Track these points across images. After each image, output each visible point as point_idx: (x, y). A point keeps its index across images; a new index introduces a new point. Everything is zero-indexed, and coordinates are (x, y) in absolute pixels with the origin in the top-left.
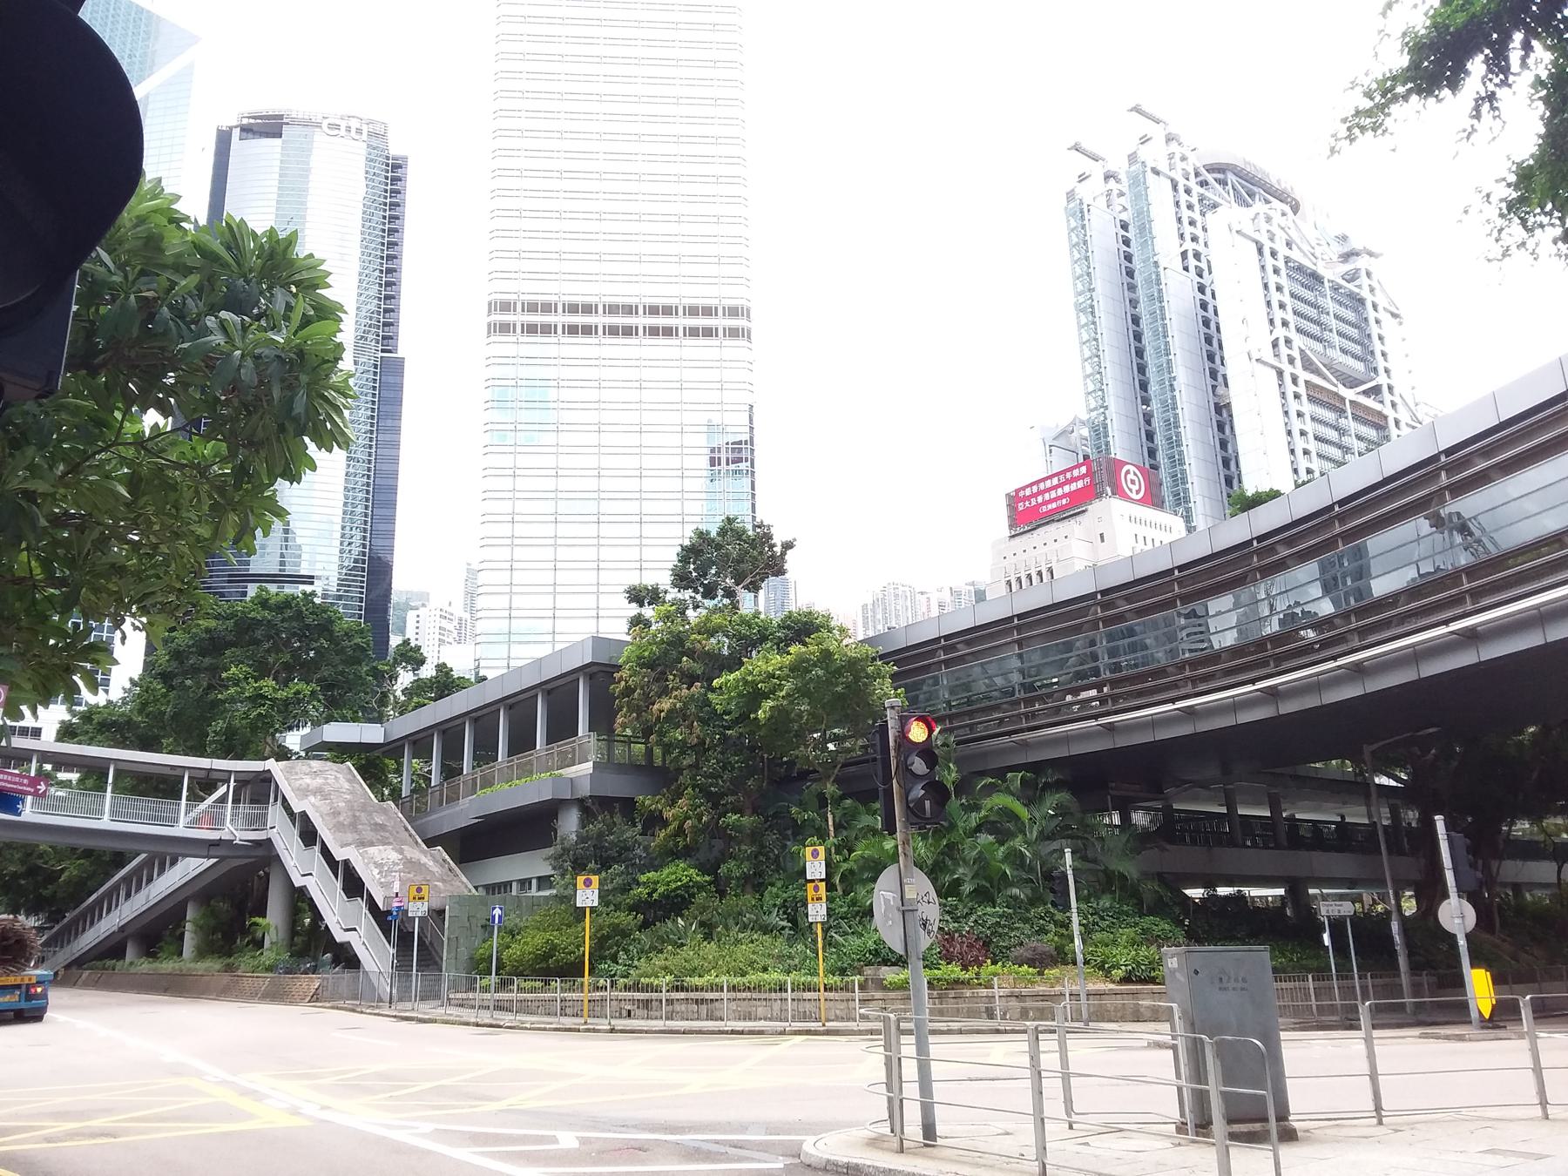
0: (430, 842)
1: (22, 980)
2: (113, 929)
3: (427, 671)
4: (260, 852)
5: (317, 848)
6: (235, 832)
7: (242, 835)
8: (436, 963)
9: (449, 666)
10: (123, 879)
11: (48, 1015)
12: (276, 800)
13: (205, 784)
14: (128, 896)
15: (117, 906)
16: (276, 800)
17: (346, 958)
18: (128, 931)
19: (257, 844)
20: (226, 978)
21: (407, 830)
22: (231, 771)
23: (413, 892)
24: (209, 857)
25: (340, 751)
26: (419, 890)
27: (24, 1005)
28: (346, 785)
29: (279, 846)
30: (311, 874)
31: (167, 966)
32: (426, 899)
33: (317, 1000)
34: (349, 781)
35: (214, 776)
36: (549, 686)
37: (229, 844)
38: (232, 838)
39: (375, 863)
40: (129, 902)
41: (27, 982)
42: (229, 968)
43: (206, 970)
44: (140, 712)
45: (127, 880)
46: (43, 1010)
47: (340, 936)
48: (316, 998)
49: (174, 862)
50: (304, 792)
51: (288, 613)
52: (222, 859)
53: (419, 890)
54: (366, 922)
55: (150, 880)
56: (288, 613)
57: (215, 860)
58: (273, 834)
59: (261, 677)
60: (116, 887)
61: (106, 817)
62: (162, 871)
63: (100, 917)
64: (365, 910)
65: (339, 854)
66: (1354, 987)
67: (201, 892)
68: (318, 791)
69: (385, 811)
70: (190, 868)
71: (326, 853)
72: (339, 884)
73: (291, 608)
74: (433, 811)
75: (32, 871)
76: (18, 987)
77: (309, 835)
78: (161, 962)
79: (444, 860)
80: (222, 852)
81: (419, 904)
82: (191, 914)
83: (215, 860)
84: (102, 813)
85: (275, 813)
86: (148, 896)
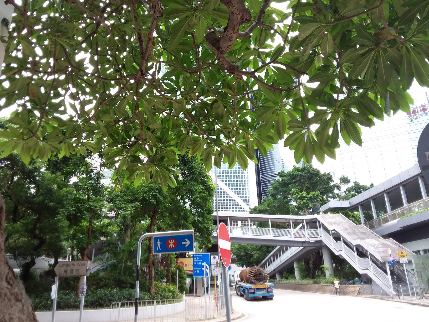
0: (386, 237)
1: (266, 286)
2: (271, 271)
3: (351, 185)
4: (318, 245)
5: (342, 242)
6: (310, 238)
7: (312, 240)
8: (403, 281)
9: (358, 182)
10: (272, 256)
11: (274, 298)
12: (320, 227)
13: (296, 224)
14: (274, 260)
15: (271, 263)
16: (320, 227)
17: (368, 280)
18: (276, 271)
19: (317, 242)
20: (316, 286)
21: (373, 234)
22: (60, 307)
23: (400, 254)
24: (300, 247)
25: (335, 210)
26: (402, 253)
27: (267, 295)
28: (343, 221)
29: (326, 242)
30: (342, 251)
31: (292, 281)
32: (406, 256)
33: (360, 294)
34: (344, 219)
35: (298, 221)
36: (404, 183)
37: (308, 242)
38: (309, 240)
39: (371, 245)
40: (275, 262)
41: (267, 287)
42: (315, 282)
43: (307, 283)
44: (268, 207)
45: (273, 256)
46: (272, 296)
47: (361, 272)
48: (359, 293)
49: (287, 249)
50: (331, 224)
51: (306, 171)
52: (304, 247)
53: (402, 253)
54: (372, 266)
55: (280, 255)
56: (306, 171)
57: (302, 248)
58: (322, 238)
59: (301, 192)
60: (270, 258)
61: (271, 235)
62: (283, 252)
63: (267, 267)
64: (371, 262)
65: (354, 242)
66: (179, 278)
67: (298, 258)
68: (335, 223)
69: (362, 228)
70: (293, 251)
71: (346, 243)
72: (355, 254)
73: (306, 170)
74: (377, 228)
75: (247, 254)
76: (265, 288)
77: (337, 238)
78: (290, 280)
79: (395, 243)
80: (304, 245)
81: (403, 258)
82: (295, 265)
83: (302, 248)
84: (270, 234)
85: (321, 231)
86: (281, 260)
